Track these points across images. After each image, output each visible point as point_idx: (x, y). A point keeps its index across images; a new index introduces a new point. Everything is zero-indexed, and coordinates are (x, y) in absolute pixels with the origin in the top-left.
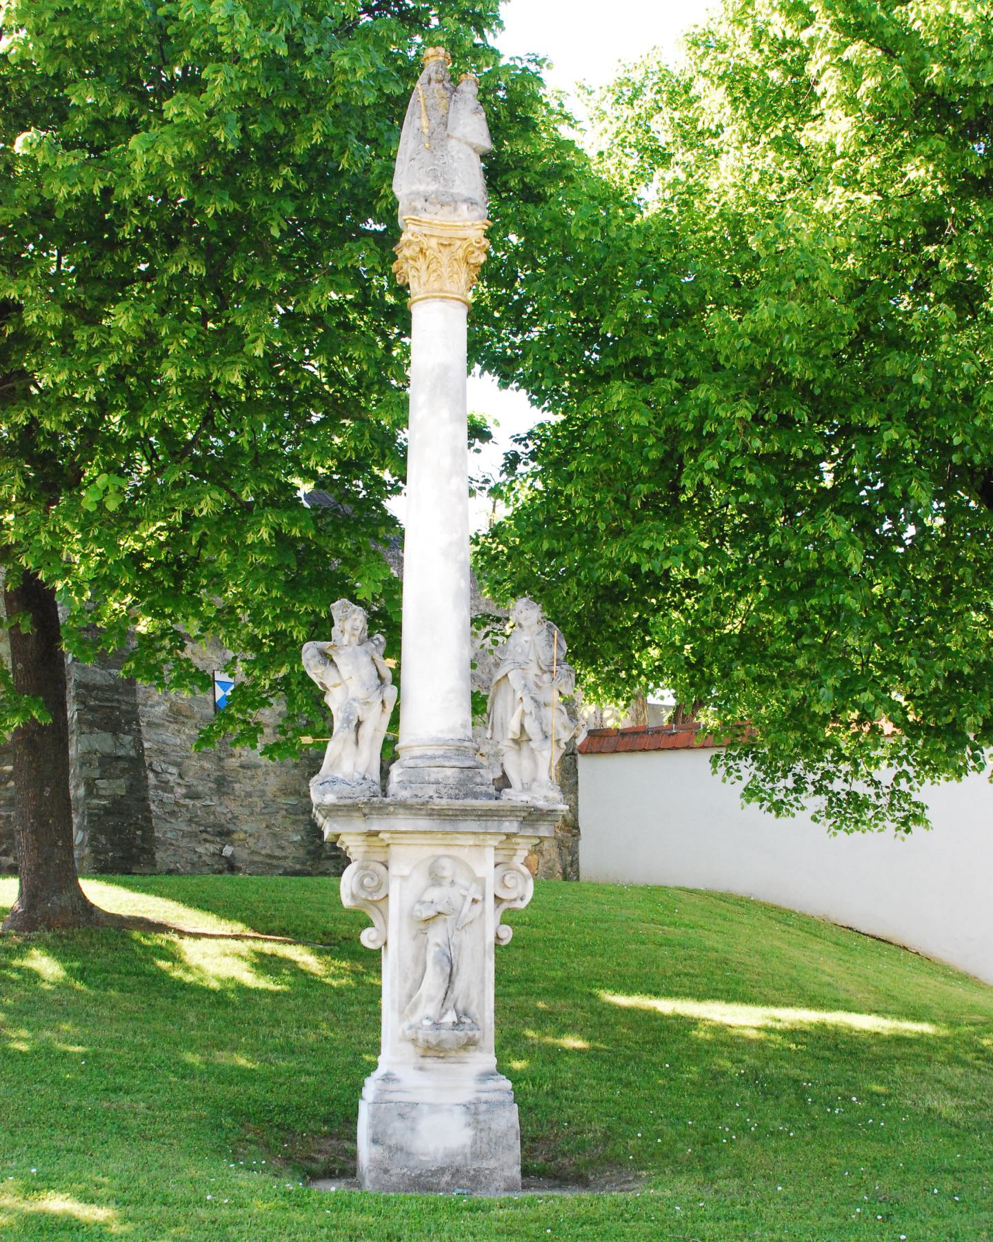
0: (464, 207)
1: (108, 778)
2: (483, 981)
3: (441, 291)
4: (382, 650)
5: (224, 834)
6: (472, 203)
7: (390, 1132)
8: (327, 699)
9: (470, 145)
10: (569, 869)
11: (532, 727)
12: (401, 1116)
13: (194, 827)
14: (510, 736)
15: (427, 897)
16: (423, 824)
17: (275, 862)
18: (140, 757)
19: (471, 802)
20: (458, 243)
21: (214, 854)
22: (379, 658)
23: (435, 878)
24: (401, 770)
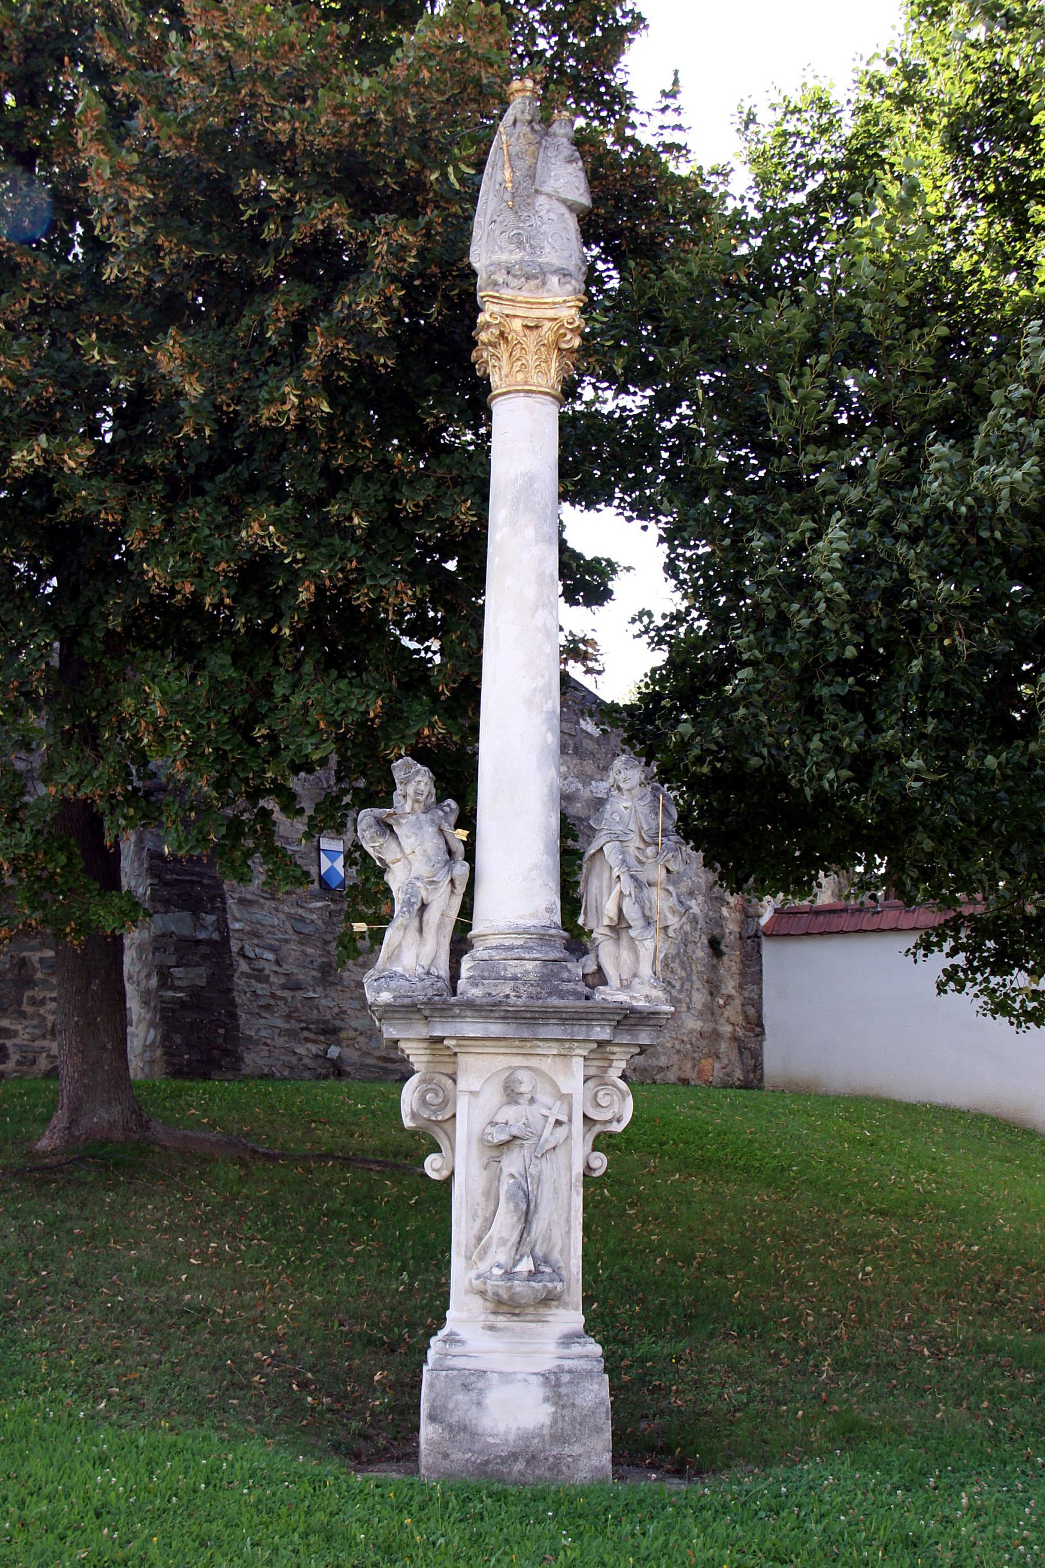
0: (555, 279)
1: (186, 966)
2: (568, 1221)
3: (526, 383)
4: (453, 819)
5: (330, 1032)
6: (564, 274)
7: (451, 1406)
8: (388, 878)
9: (564, 201)
10: (751, 1076)
11: (631, 912)
12: (466, 1387)
13: (294, 1025)
14: (606, 922)
15: (500, 1118)
16: (495, 1029)
17: (390, 1066)
18: (226, 940)
19: (555, 1001)
20: (548, 325)
21: (317, 1056)
22: (447, 829)
23: (511, 1094)
24: (472, 964)
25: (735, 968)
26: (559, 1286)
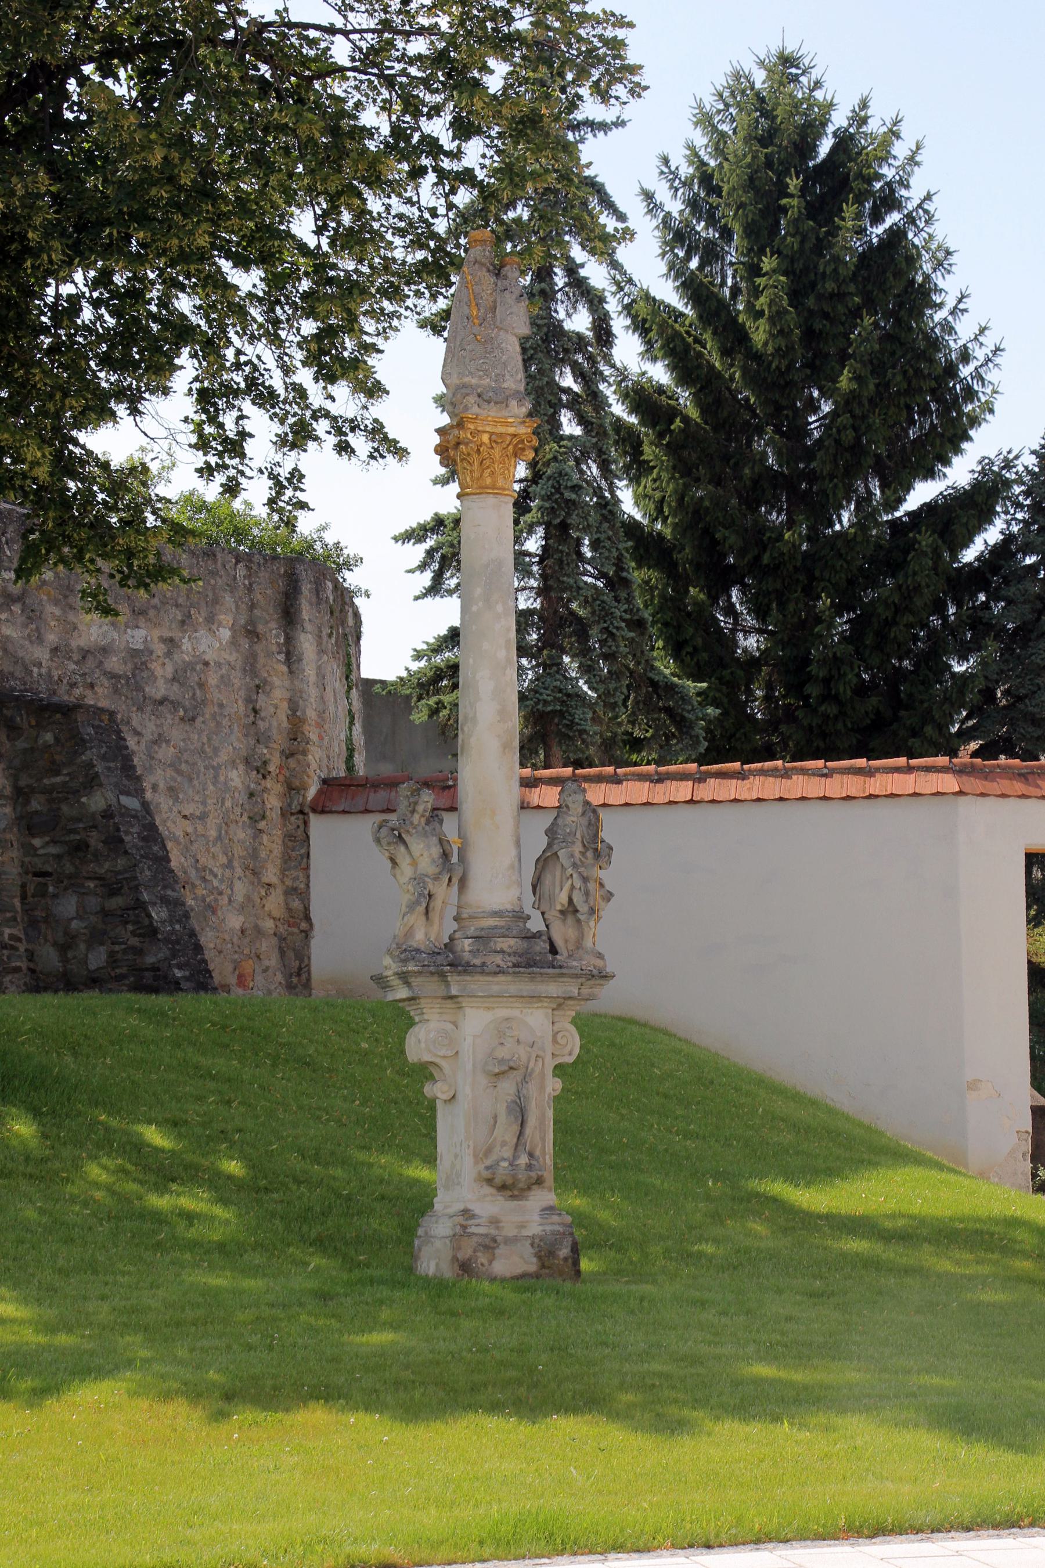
25: (277, 849)
26: (121, 862)
